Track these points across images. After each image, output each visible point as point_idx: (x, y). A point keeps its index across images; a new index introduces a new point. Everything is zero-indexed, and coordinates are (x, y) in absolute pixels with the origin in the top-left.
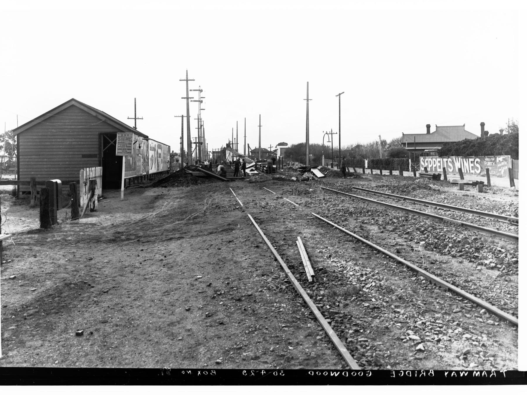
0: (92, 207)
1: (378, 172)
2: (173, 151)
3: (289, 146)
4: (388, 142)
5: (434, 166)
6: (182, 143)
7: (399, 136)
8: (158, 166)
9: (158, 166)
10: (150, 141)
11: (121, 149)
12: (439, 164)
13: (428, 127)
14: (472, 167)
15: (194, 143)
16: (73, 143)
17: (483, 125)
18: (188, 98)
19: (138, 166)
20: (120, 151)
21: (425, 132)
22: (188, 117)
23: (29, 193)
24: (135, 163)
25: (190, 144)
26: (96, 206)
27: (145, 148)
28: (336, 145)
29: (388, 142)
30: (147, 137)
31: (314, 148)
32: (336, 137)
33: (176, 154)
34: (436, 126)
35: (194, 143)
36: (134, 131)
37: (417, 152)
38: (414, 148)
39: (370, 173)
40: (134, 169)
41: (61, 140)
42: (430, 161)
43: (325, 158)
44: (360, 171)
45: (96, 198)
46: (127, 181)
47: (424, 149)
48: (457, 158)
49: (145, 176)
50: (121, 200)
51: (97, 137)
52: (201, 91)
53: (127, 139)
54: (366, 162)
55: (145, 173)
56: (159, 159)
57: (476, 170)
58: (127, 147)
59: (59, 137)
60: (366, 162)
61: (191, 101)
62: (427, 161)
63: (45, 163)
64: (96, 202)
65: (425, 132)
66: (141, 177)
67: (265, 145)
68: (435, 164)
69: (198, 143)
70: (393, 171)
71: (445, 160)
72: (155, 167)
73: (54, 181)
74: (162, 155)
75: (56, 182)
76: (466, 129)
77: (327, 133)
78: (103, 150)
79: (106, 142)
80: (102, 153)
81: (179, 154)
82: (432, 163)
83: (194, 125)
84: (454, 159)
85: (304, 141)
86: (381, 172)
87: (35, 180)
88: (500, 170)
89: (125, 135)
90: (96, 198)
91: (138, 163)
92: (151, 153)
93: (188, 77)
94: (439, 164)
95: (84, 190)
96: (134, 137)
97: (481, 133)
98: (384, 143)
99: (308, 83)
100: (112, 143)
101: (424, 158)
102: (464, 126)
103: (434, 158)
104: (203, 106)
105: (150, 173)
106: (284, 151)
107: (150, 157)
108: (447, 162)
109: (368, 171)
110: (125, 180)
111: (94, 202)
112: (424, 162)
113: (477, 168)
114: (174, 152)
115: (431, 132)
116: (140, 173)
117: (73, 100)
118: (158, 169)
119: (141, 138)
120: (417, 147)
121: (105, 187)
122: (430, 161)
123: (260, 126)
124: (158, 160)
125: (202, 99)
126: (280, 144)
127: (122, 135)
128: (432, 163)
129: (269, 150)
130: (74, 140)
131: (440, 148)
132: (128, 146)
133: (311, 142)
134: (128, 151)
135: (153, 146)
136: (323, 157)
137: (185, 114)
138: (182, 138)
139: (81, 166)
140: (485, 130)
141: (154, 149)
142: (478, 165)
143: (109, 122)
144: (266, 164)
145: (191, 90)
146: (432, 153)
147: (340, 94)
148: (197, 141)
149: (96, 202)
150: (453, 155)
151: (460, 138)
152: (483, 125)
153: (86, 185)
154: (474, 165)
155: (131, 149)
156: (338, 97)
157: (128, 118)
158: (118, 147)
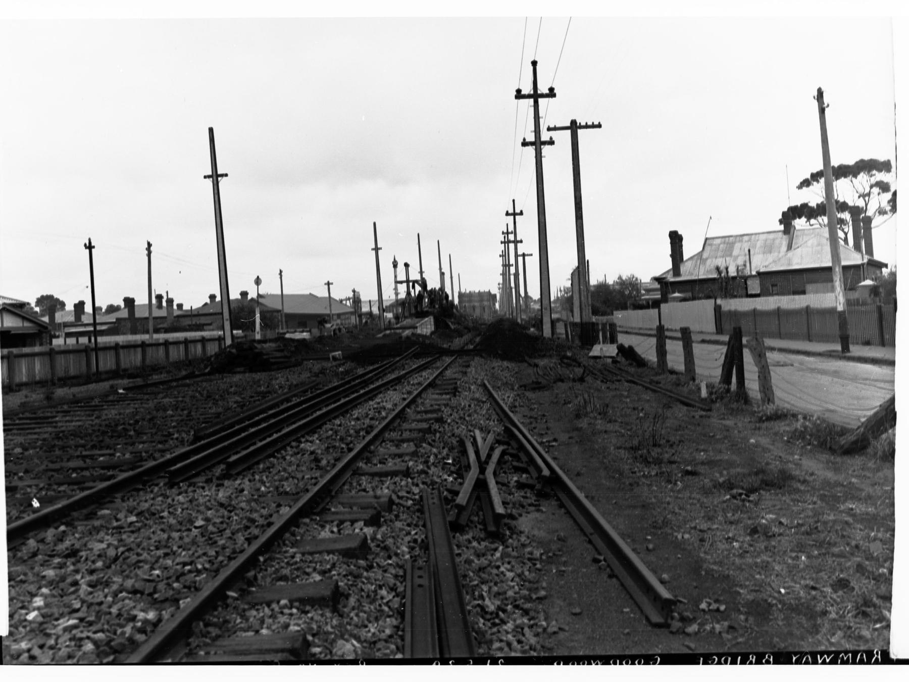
7: (307, 292)
13: (676, 239)
18: (538, 144)
99: (211, 130)
123: (215, 177)
145: (549, 129)
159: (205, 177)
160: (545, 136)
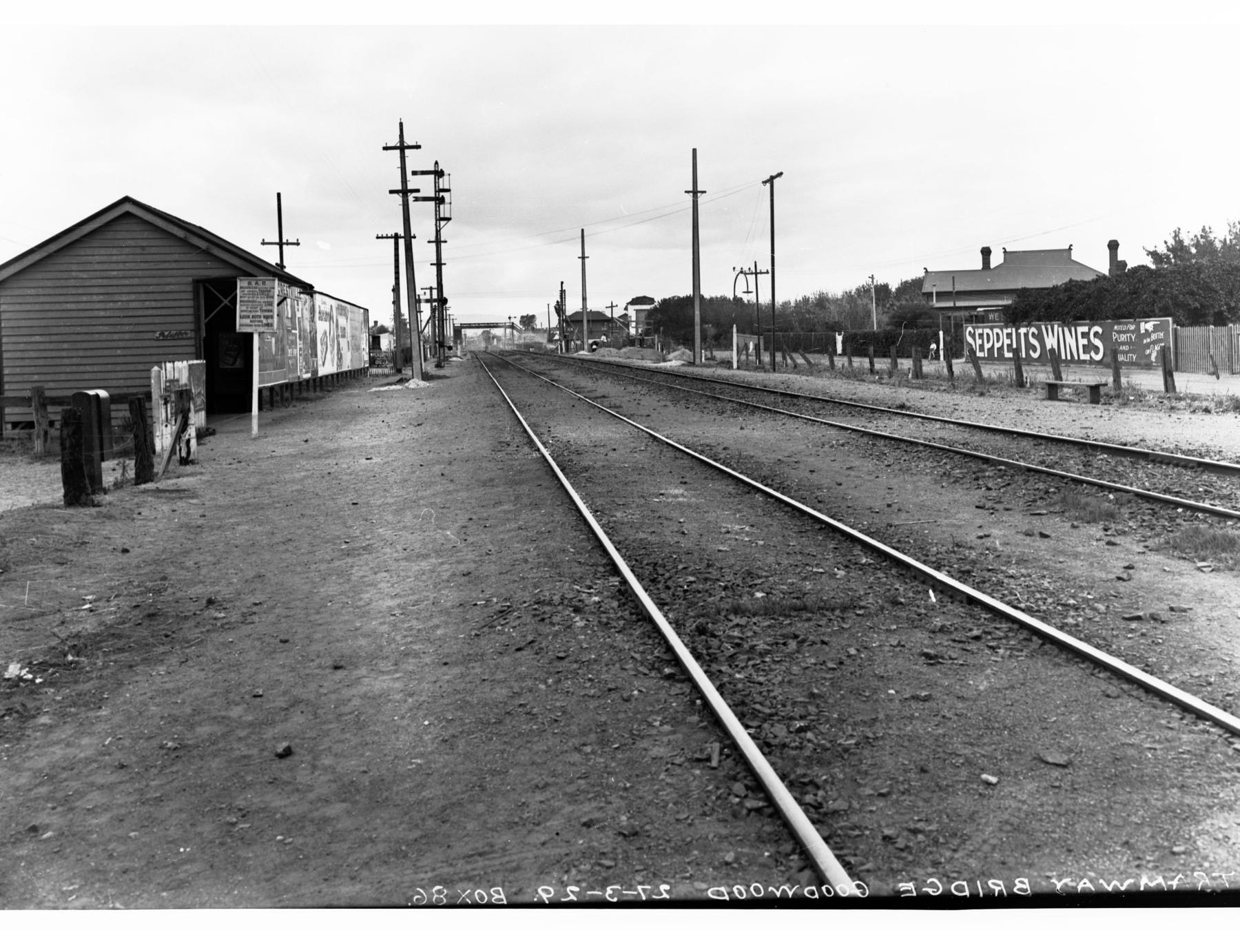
0: (184, 454)
1: (866, 362)
2: (376, 322)
3: (658, 299)
4: (894, 286)
5: (997, 345)
6: (396, 302)
8: (340, 358)
9: (340, 358)
10: (317, 297)
11: (249, 317)
12: (1007, 342)
13: (986, 252)
14: (1008, 345)
15: (427, 301)
16: (133, 305)
17: (1113, 246)
18: (405, 192)
19: (290, 358)
20: (247, 321)
21: (979, 266)
22: (409, 237)
23: (30, 425)
24: (283, 350)
25: (415, 301)
26: (192, 450)
27: (307, 314)
28: (765, 299)
29: (894, 286)
30: (311, 287)
31: (719, 303)
32: (765, 280)
33: (383, 330)
34: (1005, 252)
35: (427, 301)
36: (278, 273)
37: (957, 314)
38: (951, 304)
39: (846, 364)
40: (281, 366)
41: (101, 297)
42: (988, 334)
43: (738, 332)
44: (825, 361)
45: (192, 432)
46: (266, 394)
47: (975, 308)
48: (1049, 327)
49: (308, 381)
50: (253, 436)
51: (190, 288)
52: (439, 174)
53: (262, 292)
54: (839, 339)
55: (308, 376)
56: (341, 340)
57: (1093, 354)
58: (262, 311)
59: (96, 290)
60: (839, 339)
61: (417, 199)
62: (981, 336)
63: (64, 354)
64: (193, 442)
65: (978, 265)
66: (300, 383)
67: (596, 304)
68: (998, 341)
69: (435, 301)
70: (899, 361)
71: (1023, 331)
72: (333, 361)
73: (92, 392)
74: (348, 331)
75: (97, 395)
76: (1075, 256)
77: (741, 272)
78: (203, 321)
79: (211, 302)
80: (203, 327)
81: (390, 330)
82: (993, 338)
83: (423, 252)
84: (1043, 327)
85: (686, 290)
86: (872, 363)
87: (43, 393)
88: (1148, 352)
89: (257, 283)
90: (192, 432)
91: (290, 351)
92: (322, 326)
93: (405, 139)
94: (1007, 342)
95: (164, 415)
96: (277, 287)
97: (1108, 267)
98: (883, 290)
99: (694, 151)
100: (226, 302)
101: (974, 328)
102: (1070, 249)
103: (996, 327)
104: (445, 210)
105: (320, 374)
106: (643, 315)
107: (319, 336)
108: (1026, 335)
109: (840, 362)
110: (260, 391)
111: (188, 441)
112: (973, 336)
113: (1097, 350)
114: (379, 325)
115: (993, 265)
116: (295, 375)
117: (127, 199)
118: (339, 365)
119: (297, 290)
120: (960, 300)
121: (213, 410)
122: (988, 334)
123: (695, 192)
124: (339, 344)
125: (441, 194)
126: (636, 301)
127: (250, 283)
128: (993, 338)
129: (608, 313)
130: (133, 297)
131: (1010, 302)
132: (264, 308)
133: (708, 292)
134: (265, 321)
135: (326, 308)
136: (735, 330)
137: (401, 232)
138: (396, 290)
139: (154, 359)
140: (1120, 258)
141: (329, 317)
142: (1097, 342)
143: (216, 252)
144: (1018, 335)
145: (414, 173)
146: (991, 316)
147: (772, 179)
148: (435, 296)
149: (193, 442)
150: (1039, 320)
151: (1054, 279)
152: (1113, 246)
153: (166, 403)
154: (1089, 341)
155: (272, 317)
156: (768, 185)
157: (264, 243)
158: (242, 311)
159: (392, 192)
160: (410, 186)
